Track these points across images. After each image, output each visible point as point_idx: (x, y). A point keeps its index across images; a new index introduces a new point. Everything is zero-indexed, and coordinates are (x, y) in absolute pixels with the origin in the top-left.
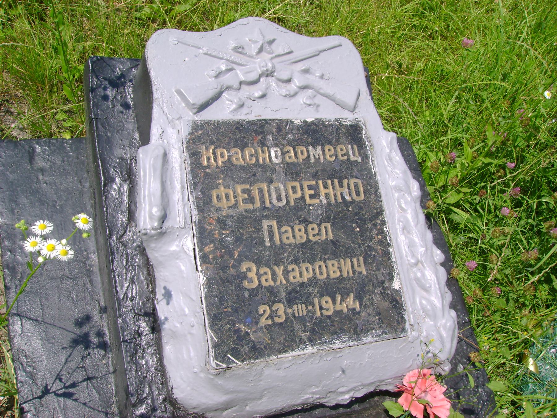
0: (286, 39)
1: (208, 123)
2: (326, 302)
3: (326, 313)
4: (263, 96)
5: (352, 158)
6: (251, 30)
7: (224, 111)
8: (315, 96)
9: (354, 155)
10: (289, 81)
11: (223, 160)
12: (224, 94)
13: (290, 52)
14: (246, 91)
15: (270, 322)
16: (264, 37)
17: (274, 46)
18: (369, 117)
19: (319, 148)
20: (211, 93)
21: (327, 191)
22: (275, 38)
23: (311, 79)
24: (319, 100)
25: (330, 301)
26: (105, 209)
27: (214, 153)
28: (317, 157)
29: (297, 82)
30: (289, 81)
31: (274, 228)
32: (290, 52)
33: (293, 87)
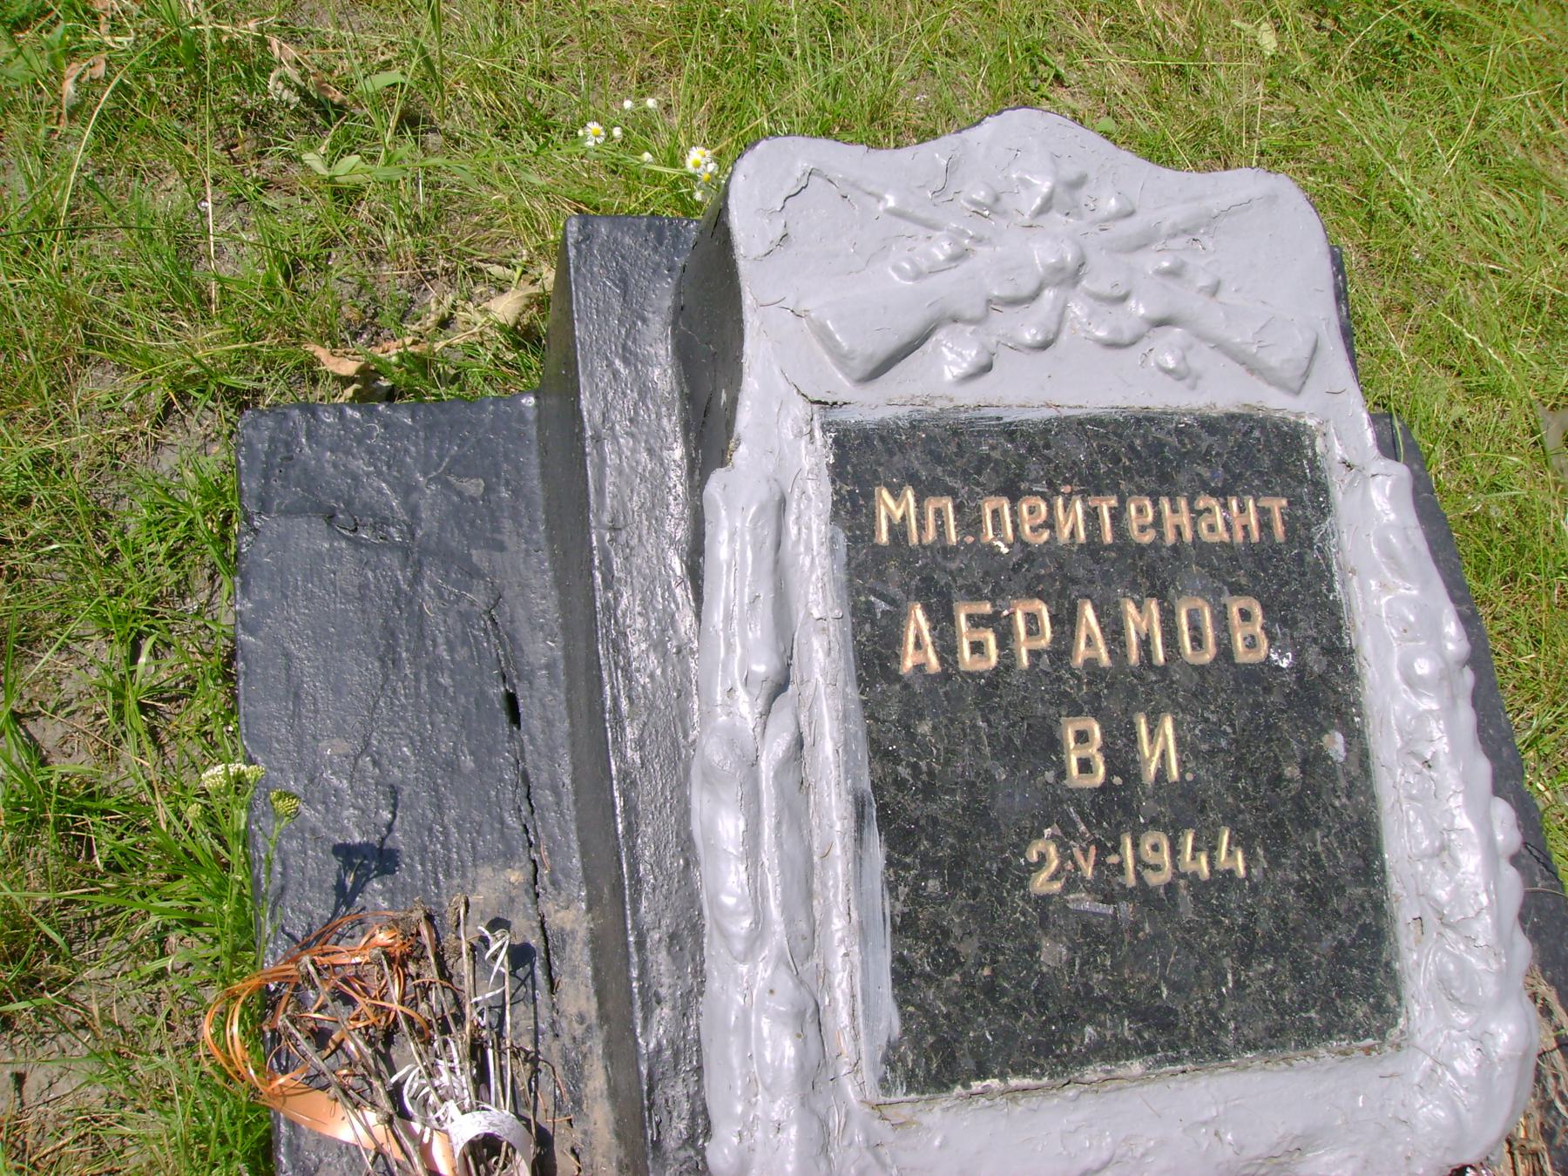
0: (1126, 182)
2: (1155, 848)
4: (1044, 346)
6: (1022, 149)
7: (943, 377)
17: (1083, 194)
18: (1343, 428)
20: (908, 326)
21: (1176, 520)
23: (1187, 299)
26: (635, 973)
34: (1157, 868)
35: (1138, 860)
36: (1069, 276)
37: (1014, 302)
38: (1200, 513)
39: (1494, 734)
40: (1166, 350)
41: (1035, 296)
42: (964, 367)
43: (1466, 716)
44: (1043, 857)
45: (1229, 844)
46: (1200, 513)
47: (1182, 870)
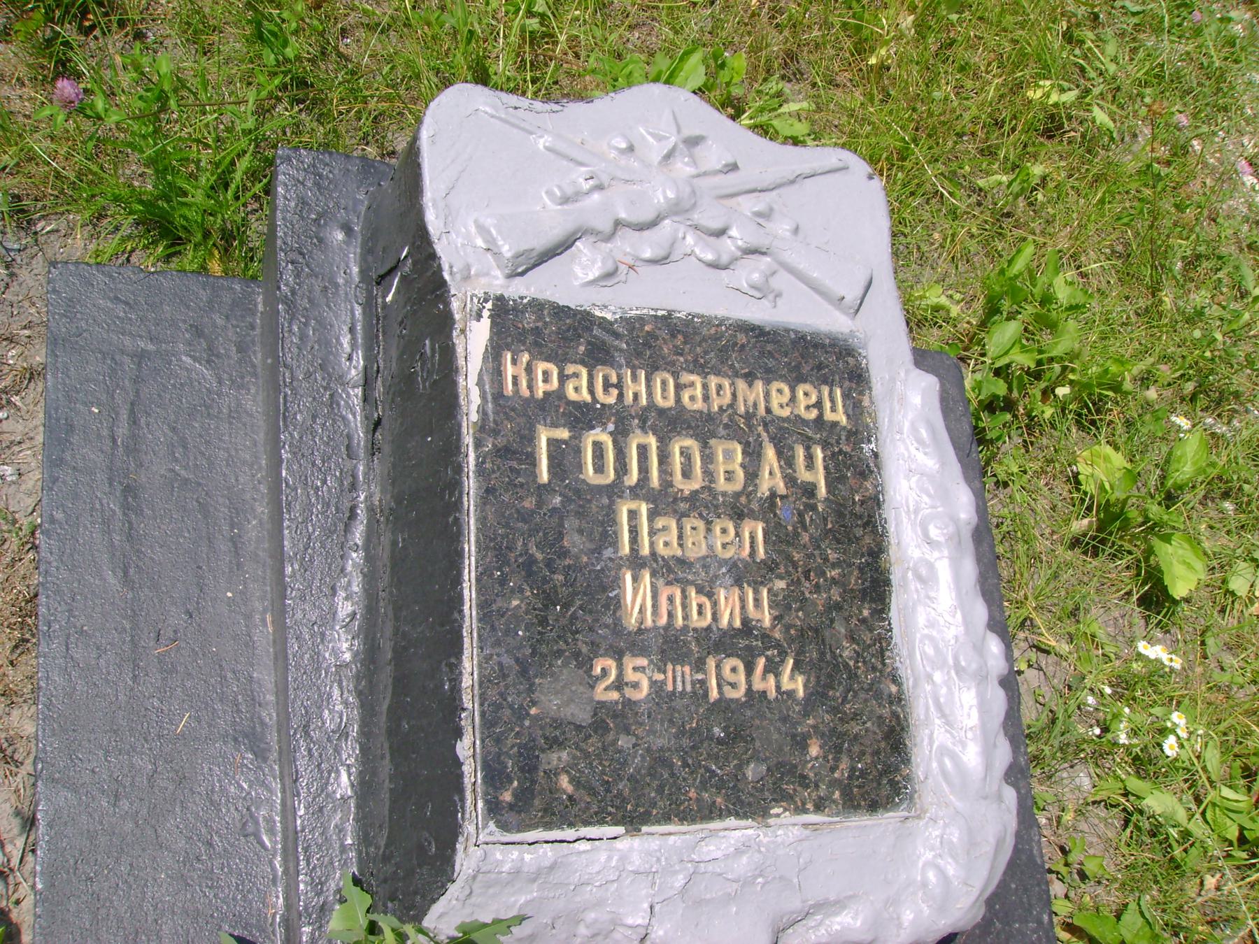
0: (727, 139)
1: (537, 306)
2: (734, 670)
3: (731, 694)
5: (829, 416)
8: (774, 273)
9: (833, 409)
10: (721, 233)
11: (549, 388)
12: (577, 243)
13: (733, 167)
14: (628, 245)
15: (614, 695)
16: (679, 131)
19: (759, 385)
22: (704, 134)
24: (782, 281)
25: (741, 667)
27: (529, 369)
28: (750, 403)
29: (739, 236)
30: (721, 233)
31: (622, 526)
32: (733, 167)
33: (728, 247)
34: (733, 686)
35: (719, 677)
36: (677, 209)
37: (641, 227)
38: (568, 377)
39: (993, 585)
40: (751, 272)
41: (653, 224)
42: (594, 273)
43: (970, 568)
44: (605, 672)
45: (792, 670)
46: (568, 377)
47: (783, 689)
